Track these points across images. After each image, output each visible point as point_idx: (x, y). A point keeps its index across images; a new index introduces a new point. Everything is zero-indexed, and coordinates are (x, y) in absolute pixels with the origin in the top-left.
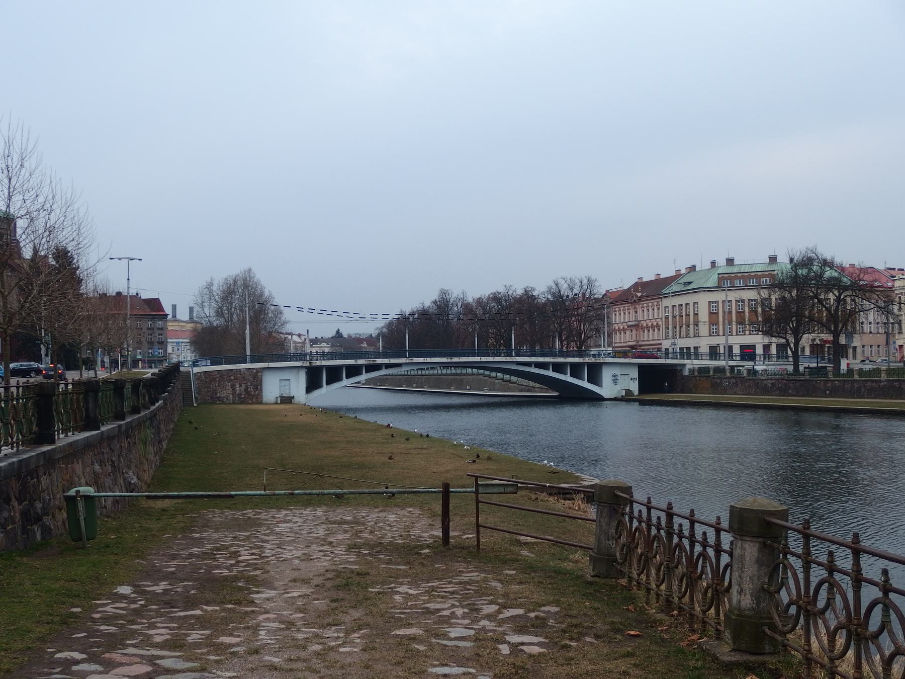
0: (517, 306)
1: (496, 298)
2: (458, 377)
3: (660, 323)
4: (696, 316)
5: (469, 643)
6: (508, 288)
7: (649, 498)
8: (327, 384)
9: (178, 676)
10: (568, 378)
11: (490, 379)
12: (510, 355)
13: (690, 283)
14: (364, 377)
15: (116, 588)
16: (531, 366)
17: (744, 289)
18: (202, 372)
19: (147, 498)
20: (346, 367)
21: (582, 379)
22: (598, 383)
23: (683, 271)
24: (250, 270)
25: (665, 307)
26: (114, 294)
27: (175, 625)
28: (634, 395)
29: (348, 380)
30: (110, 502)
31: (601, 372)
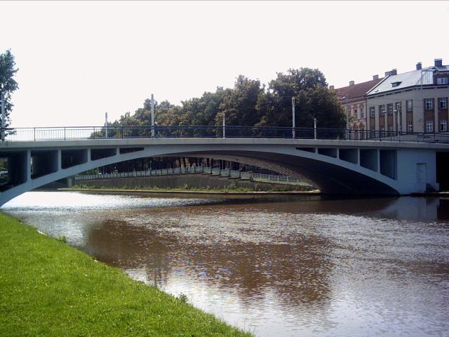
0: (67, 286)
1: (207, 96)
2: (170, 177)
3: (365, 123)
4: (410, 114)
5: (192, 233)
6: (220, 89)
7: (152, 96)
8: (394, 178)
9: (409, 192)
10: (356, 167)
11: (211, 178)
12: (289, 135)
13: (398, 83)
14: (90, 165)
15: (289, 76)
16: (314, 152)
17: (433, 88)
18: (390, 177)
19: (376, 77)
20: (381, 151)
21: (372, 168)
22: (393, 176)
23: (382, 75)
24: (240, 78)
25: (371, 108)
26: (270, 295)
27: (180, 286)
28: (435, 190)
29: (93, 162)
30: (74, 233)
31: (395, 163)
